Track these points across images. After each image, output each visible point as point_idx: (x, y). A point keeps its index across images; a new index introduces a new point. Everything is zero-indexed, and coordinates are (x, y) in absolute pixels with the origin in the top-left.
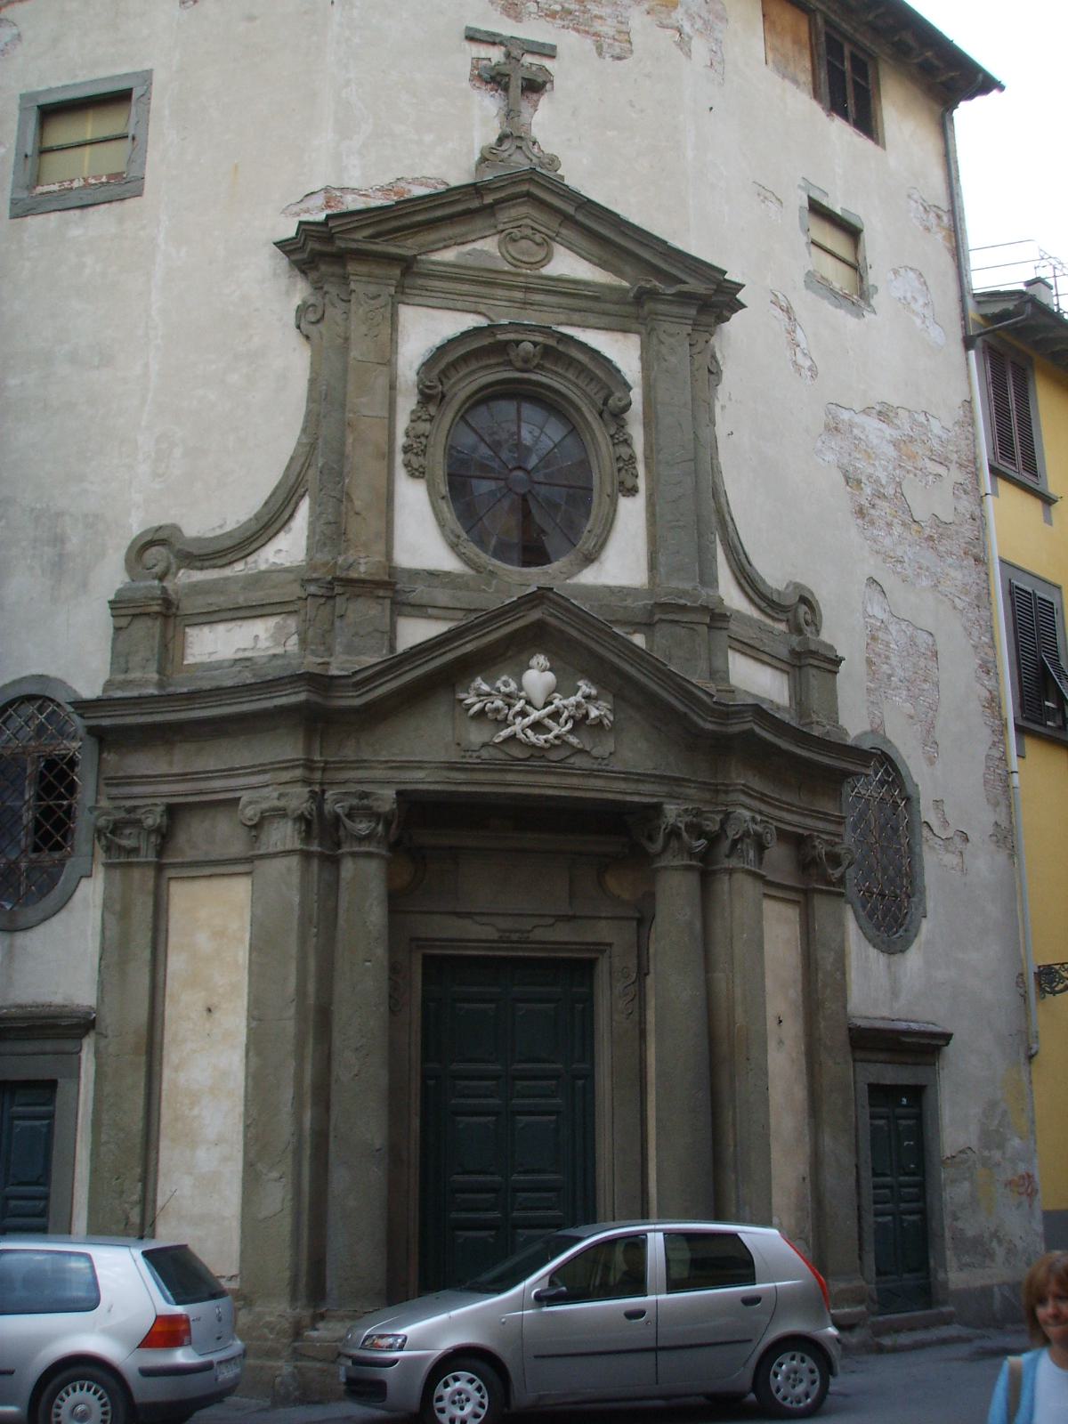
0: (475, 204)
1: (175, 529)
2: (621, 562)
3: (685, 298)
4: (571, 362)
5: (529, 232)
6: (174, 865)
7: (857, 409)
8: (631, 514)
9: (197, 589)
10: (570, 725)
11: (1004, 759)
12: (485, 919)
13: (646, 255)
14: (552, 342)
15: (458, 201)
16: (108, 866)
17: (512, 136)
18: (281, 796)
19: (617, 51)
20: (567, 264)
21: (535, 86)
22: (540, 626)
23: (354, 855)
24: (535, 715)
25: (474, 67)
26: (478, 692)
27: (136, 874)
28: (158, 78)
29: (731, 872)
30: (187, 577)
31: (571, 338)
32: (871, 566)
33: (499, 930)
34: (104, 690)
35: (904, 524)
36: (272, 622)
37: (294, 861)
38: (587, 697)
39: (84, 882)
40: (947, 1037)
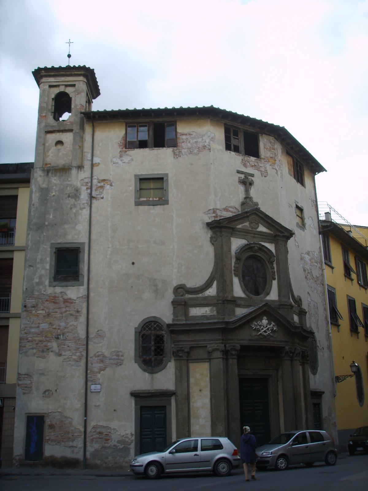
0: (246, 215)
1: (184, 285)
2: (273, 296)
3: (284, 236)
4: (264, 251)
5: (255, 221)
6: (190, 360)
8: (275, 283)
9: (190, 299)
10: (270, 331)
11: (328, 330)
13: (277, 227)
14: (260, 247)
16: (175, 360)
17: (248, 197)
18: (217, 346)
19: (265, 175)
20: (262, 228)
21: (251, 184)
22: (265, 310)
23: (232, 358)
24: (265, 329)
25: (239, 179)
26: (254, 325)
28: (170, 176)
29: (296, 360)
30: (188, 296)
34: (173, 321)
36: (210, 308)
37: (221, 360)
38: (273, 325)
39: (169, 363)
40: (324, 392)
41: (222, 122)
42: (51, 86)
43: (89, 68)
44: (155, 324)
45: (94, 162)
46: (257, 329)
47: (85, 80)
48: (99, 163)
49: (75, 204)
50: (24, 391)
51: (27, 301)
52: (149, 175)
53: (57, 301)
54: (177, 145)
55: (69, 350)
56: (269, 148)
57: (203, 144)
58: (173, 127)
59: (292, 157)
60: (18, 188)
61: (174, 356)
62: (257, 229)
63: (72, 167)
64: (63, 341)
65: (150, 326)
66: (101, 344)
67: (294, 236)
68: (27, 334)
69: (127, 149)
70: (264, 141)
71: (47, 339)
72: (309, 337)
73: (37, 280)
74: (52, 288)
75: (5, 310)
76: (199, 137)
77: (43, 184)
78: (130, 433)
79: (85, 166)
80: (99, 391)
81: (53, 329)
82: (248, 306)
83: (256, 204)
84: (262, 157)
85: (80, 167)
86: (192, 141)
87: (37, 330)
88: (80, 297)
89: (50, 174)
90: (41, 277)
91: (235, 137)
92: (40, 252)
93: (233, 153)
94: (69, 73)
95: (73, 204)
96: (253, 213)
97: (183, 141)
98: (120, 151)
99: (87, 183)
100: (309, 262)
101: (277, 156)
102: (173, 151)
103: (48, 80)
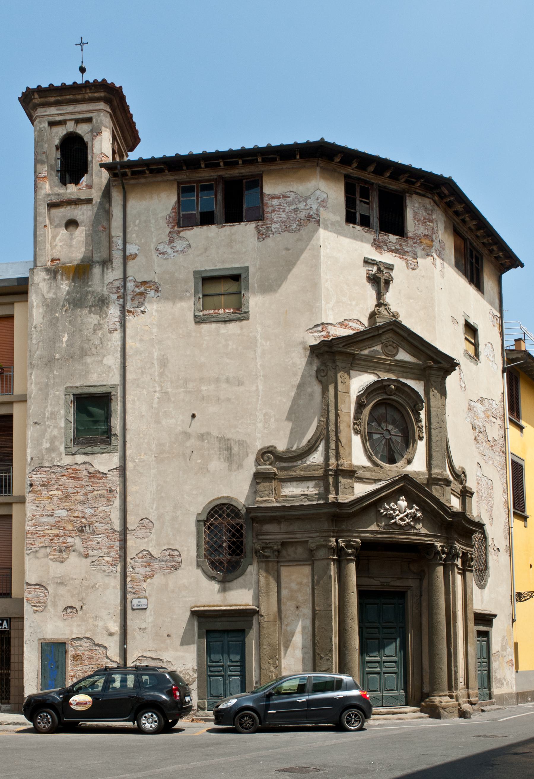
0: (377, 333)
4: (404, 392)
5: (391, 343)
6: (282, 561)
7: (476, 401)
8: (421, 446)
12: (377, 579)
14: (400, 385)
15: (371, 332)
16: (258, 562)
19: (413, 267)
20: (403, 356)
24: (401, 516)
26: (387, 508)
27: (270, 564)
28: (251, 270)
31: (406, 384)
32: (479, 458)
33: (381, 582)
35: (486, 442)
38: (416, 510)
39: (250, 566)
40: (495, 616)
41: (342, 171)
42: (52, 124)
43: (113, 84)
44: (228, 508)
45: (128, 253)
46: (388, 516)
47: (109, 110)
48: (136, 255)
49: (100, 324)
50: (35, 608)
51: (34, 476)
52: (216, 270)
53: (80, 476)
54: (264, 217)
55: (100, 548)
56: (422, 219)
57: (308, 213)
58: (258, 189)
59: (463, 239)
60: (12, 304)
61: (257, 556)
62: (375, 383)
63: (93, 262)
64: (88, 536)
65: (221, 512)
66: (146, 540)
67: (457, 368)
68: (36, 525)
69: (180, 227)
70: (414, 206)
71: (67, 532)
72: (475, 532)
73: (48, 445)
74: (70, 457)
75: (5, 493)
76: (301, 200)
77: (48, 292)
78: (191, 667)
79: (114, 260)
80: (145, 607)
81: (74, 517)
82: (376, 481)
83: (395, 315)
84: (409, 236)
85: (106, 263)
86: (288, 208)
87: (51, 520)
88: (113, 469)
89: (59, 277)
90: (52, 440)
91: (363, 200)
92: (49, 401)
93: (358, 228)
94: (79, 97)
95: (97, 324)
96: (389, 330)
97: (273, 209)
98: (170, 232)
99: (118, 287)
100: (482, 415)
101: (437, 234)
102: (257, 227)
103: (46, 111)
